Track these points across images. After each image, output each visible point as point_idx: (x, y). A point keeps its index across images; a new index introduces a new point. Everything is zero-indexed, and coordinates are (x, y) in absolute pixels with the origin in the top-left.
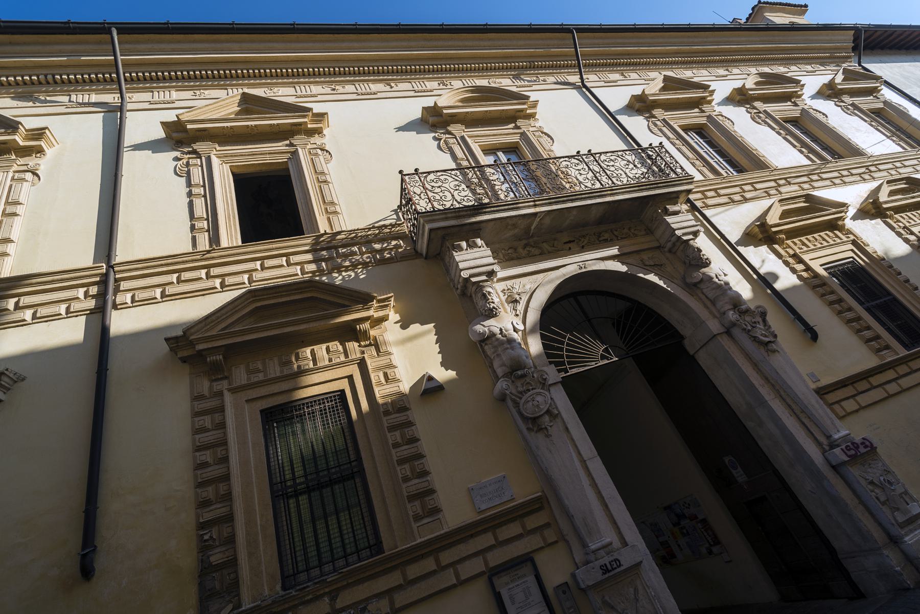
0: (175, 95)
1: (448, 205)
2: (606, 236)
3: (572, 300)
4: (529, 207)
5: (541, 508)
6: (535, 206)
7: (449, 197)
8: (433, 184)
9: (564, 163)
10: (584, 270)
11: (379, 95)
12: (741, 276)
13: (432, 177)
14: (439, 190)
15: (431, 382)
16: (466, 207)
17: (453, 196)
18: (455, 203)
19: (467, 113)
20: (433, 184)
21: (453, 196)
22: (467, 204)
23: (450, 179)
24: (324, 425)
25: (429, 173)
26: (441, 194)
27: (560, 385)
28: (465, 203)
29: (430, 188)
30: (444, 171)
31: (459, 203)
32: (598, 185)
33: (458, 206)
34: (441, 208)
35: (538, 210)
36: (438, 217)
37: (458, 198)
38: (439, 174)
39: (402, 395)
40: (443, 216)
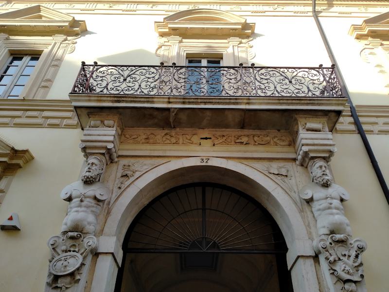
0: (355, 9)
1: (269, 93)
2: (245, 140)
3: (199, 190)
4: (163, 102)
7: (272, 88)
8: (262, 77)
10: (204, 164)
11: (267, 14)
13: (263, 71)
14: (266, 81)
17: (275, 87)
18: (276, 92)
19: (207, 29)
20: (262, 77)
21: (275, 87)
22: (285, 95)
23: (278, 74)
24: (181, 243)
28: (283, 94)
29: (258, 79)
30: (115, 66)
31: (278, 93)
33: (277, 95)
35: (170, 106)
36: (83, 98)
37: (279, 89)
38: (269, 69)
39: (345, 229)
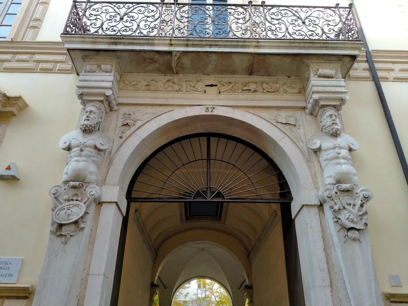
1: (280, 36)
2: (253, 87)
5: (25, 298)
6: (187, 45)
7: (284, 29)
8: (273, 16)
9: (315, 14)
10: (209, 113)
12: (128, 156)
13: (274, 10)
14: (277, 22)
15: (8, 171)
16: (295, 39)
18: (287, 34)
20: (273, 16)
21: (287, 29)
22: (298, 37)
23: (290, 14)
25: (273, 6)
26: (277, 26)
27: (279, 204)
28: (295, 36)
29: (269, 19)
31: (290, 35)
32: (324, 37)
34: (273, 37)
37: (291, 31)
38: (281, 8)
40: (288, 45)
